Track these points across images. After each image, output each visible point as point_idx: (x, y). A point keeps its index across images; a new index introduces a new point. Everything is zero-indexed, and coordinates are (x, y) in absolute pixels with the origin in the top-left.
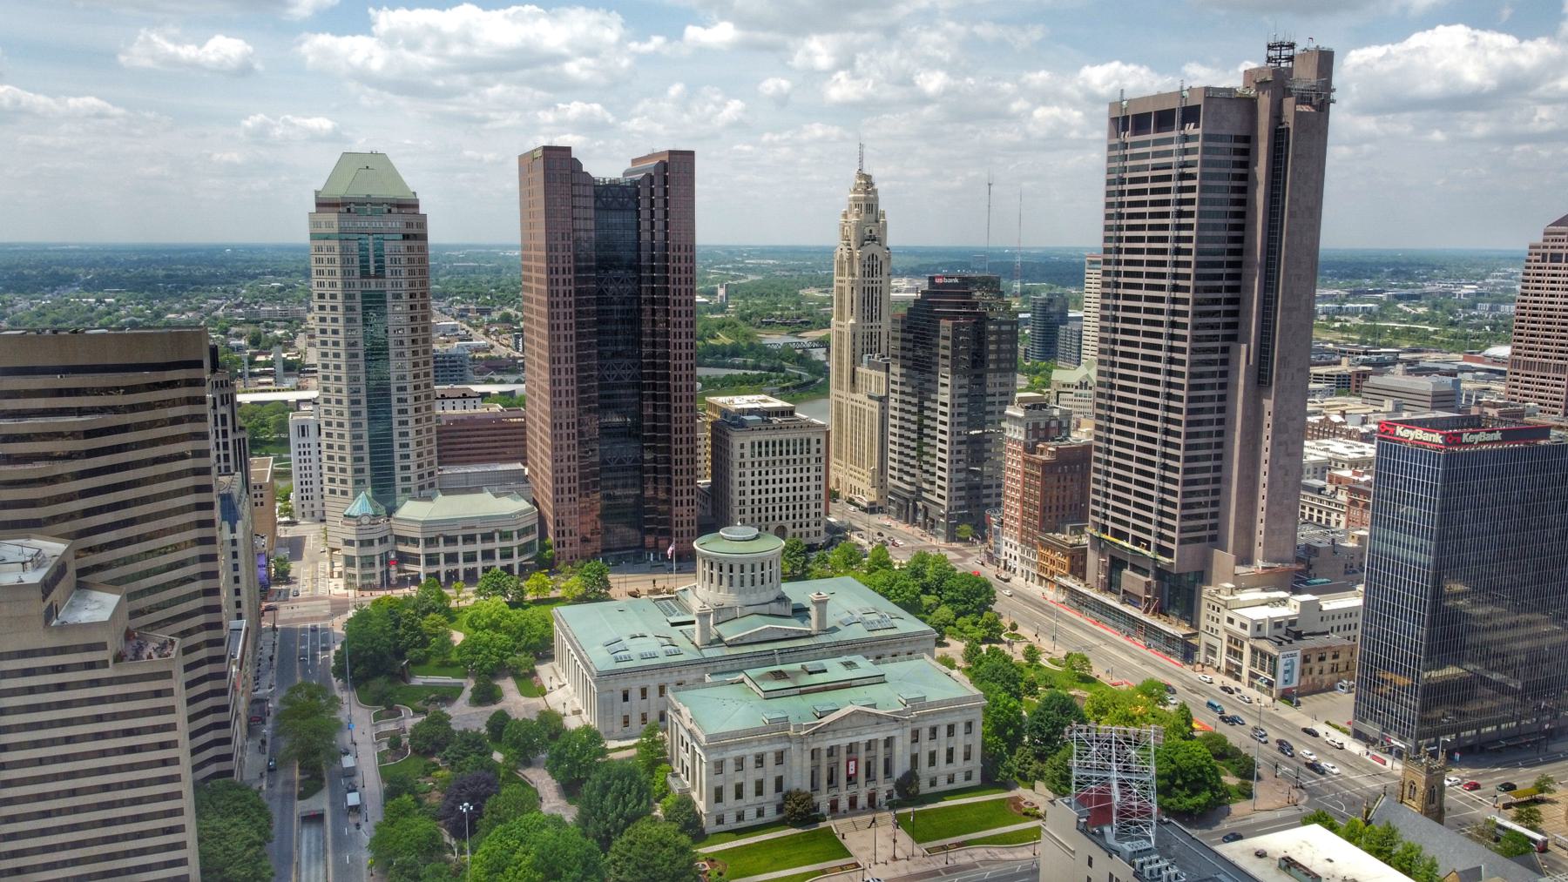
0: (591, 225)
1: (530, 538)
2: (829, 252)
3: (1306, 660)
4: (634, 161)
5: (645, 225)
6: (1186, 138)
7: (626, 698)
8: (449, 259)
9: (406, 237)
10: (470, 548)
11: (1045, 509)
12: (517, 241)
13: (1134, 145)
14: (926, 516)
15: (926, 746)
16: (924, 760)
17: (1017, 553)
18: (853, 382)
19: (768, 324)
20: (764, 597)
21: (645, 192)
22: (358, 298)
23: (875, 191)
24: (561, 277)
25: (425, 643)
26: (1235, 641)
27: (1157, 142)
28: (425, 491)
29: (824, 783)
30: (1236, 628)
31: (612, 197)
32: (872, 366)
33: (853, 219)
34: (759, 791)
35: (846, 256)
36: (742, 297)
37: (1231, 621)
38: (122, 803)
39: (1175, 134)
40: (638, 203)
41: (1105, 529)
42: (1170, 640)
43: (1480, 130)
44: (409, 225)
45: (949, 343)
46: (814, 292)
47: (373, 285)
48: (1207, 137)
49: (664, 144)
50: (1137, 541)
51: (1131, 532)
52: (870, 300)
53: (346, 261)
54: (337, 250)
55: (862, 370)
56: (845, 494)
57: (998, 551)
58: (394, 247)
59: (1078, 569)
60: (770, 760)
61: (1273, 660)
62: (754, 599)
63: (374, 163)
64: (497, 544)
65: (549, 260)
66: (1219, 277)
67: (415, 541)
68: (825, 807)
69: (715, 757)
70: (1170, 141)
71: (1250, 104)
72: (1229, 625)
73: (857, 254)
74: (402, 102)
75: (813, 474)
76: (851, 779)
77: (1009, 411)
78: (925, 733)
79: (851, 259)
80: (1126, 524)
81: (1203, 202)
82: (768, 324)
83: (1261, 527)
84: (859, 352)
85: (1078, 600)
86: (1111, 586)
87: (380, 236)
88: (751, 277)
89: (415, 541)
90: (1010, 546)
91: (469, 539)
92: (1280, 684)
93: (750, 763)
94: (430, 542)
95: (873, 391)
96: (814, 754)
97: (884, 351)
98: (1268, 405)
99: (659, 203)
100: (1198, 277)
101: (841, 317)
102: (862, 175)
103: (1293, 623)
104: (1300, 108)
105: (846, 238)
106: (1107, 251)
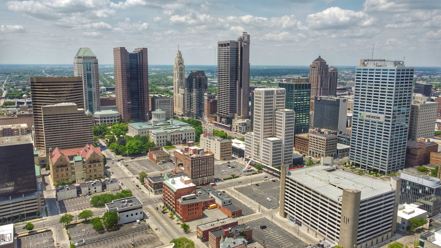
0: (129, 61)
1: (119, 118)
2: (172, 67)
3: (246, 128)
4: (135, 49)
5: (138, 61)
6: (228, 48)
7: (142, 133)
8: (67, 69)
9: (95, 63)
10: (108, 119)
11: (211, 111)
12: (113, 64)
13: (221, 49)
14: (192, 115)
15: (187, 136)
16: (187, 138)
17: (207, 119)
18: (178, 92)
19: (159, 85)
20: (163, 120)
21: (138, 55)
22: (86, 74)
23: (181, 54)
24: (124, 70)
25: (105, 131)
26: (237, 126)
27: (224, 49)
28: (99, 110)
29: (173, 140)
30: (237, 124)
31: (133, 56)
32: (182, 88)
33: (177, 60)
34: (163, 141)
35: (176, 67)
36: (152, 78)
38: (82, 135)
39: (226, 47)
40: (137, 57)
41: (219, 112)
42: (228, 128)
43: (345, 35)
44: (95, 61)
45: (195, 83)
46: (171, 77)
47: (89, 72)
48: (231, 48)
49: (142, 47)
50: (224, 113)
51: (223, 112)
52: (181, 76)
53: (84, 68)
54: (82, 66)
55: (180, 89)
56: (177, 114)
57: (204, 119)
58: (93, 66)
59: (216, 120)
60: (165, 137)
61: (241, 128)
62: (161, 120)
63: (87, 50)
64: (113, 119)
65: (122, 67)
66: (234, 70)
67: (98, 118)
68: (173, 144)
69: (157, 136)
70: (226, 48)
71: (238, 43)
73: (178, 67)
74: (39, 20)
75: (170, 107)
76: (176, 140)
77: (205, 94)
78: (187, 134)
79: (177, 68)
80: (222, 111)
81: (230, 58)
82: (159, 85)
83: (242, 110)
84: (179, 86)
85: (216, 124)
86: (220, 122)
87: (90, 64)
88: (153, 73)
89: (98, 118)
90: (206, 118)
91: (108, 118)
92: (242, 132)
93: (162, 137)
94: (101, 118)
95: (182, 93)
96: (171, 136)
97: (184, 85)
98: (242, 90)
99: (141, 57)
100: (230, 70)
101: (175, 79)
102: (179, 51)
103: (245, 123)
104: (244, 44)
105: (176, 63)
106: (218, 66)
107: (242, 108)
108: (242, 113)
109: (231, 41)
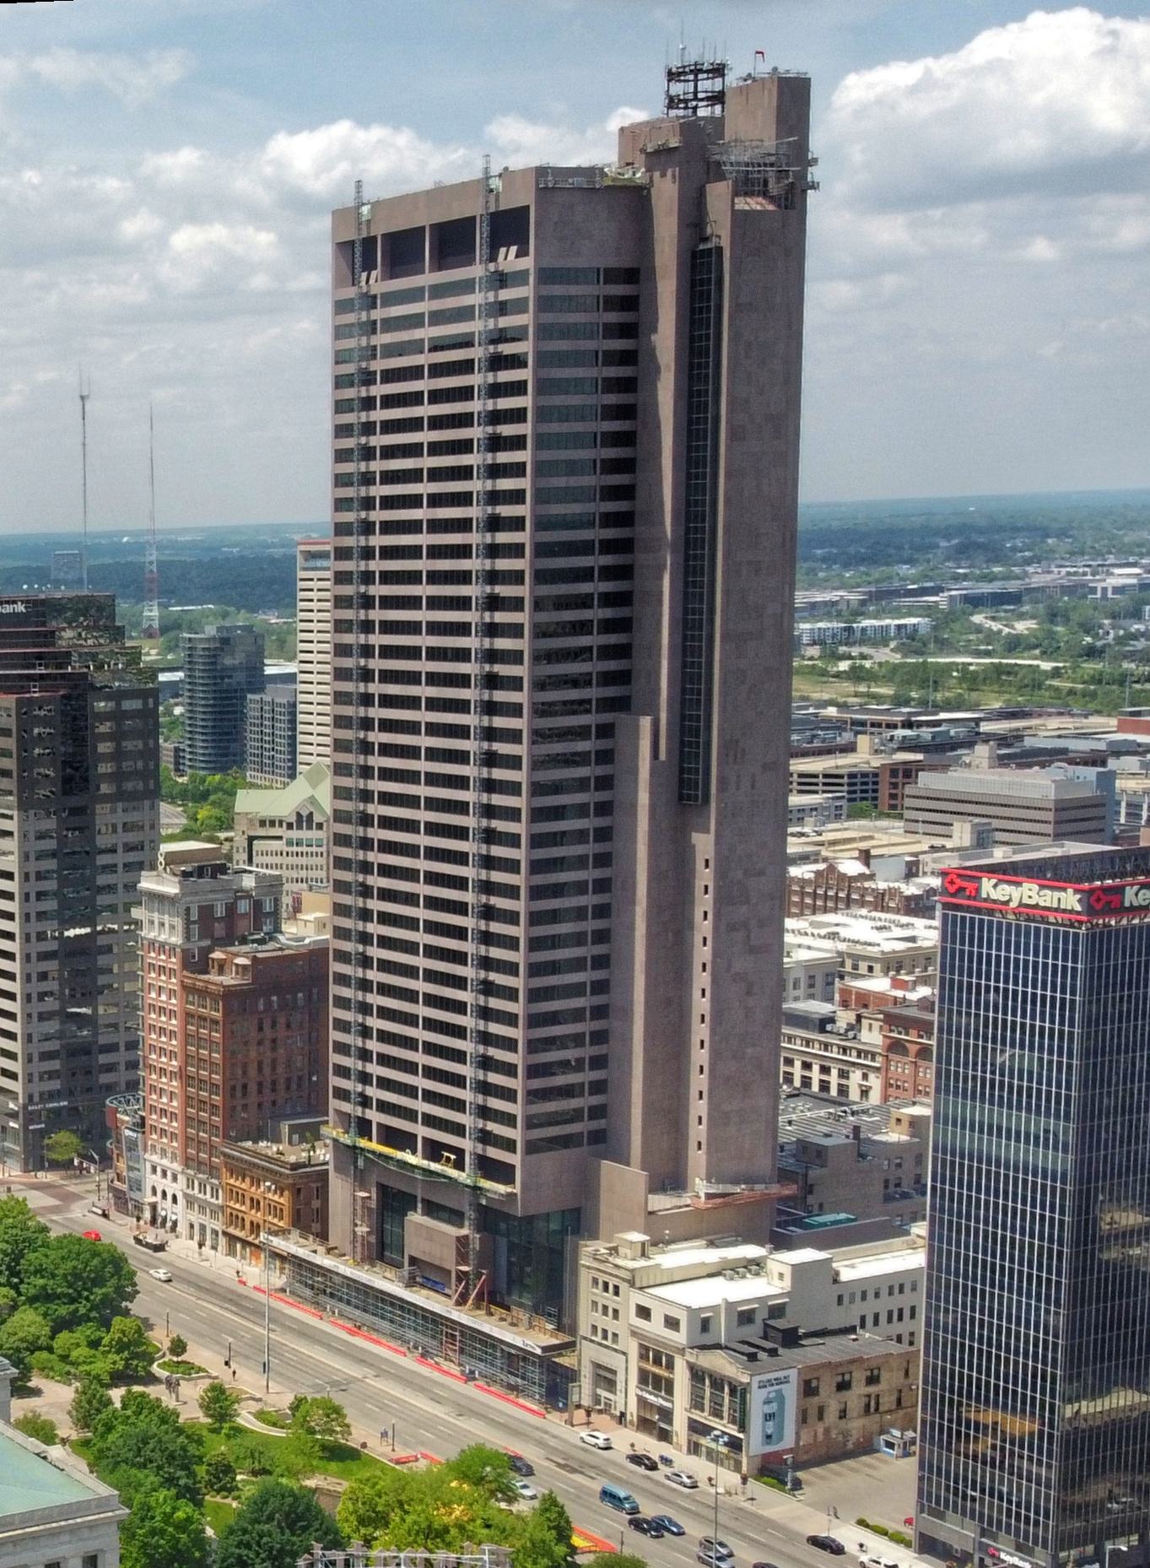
3: (809, 1389)
6: (501, 280)
13: (391, 299)
17: (178, 1188)
26: (655, 1357)
30: (655, 1327)
37: (644, 1313)
39: (477, 271)
41: (364, 1127)
42: (516, 1360)
48: (546, 276)
57: (137, 1186)
61: (739, 1392)
66: (585, 575)
70: (467, 286)
71: (637, 199)
72: (641, 1323)
81: (542, 414)
86: (382, 1249)
92: (755, 1444)
98: (704, 844)
100: (541, 577)
103: (777, 1311)
104: (742, 204)
106: (341, 529)
107: (699, 1082)
108: (697, 1160)
109: (549, 181)
